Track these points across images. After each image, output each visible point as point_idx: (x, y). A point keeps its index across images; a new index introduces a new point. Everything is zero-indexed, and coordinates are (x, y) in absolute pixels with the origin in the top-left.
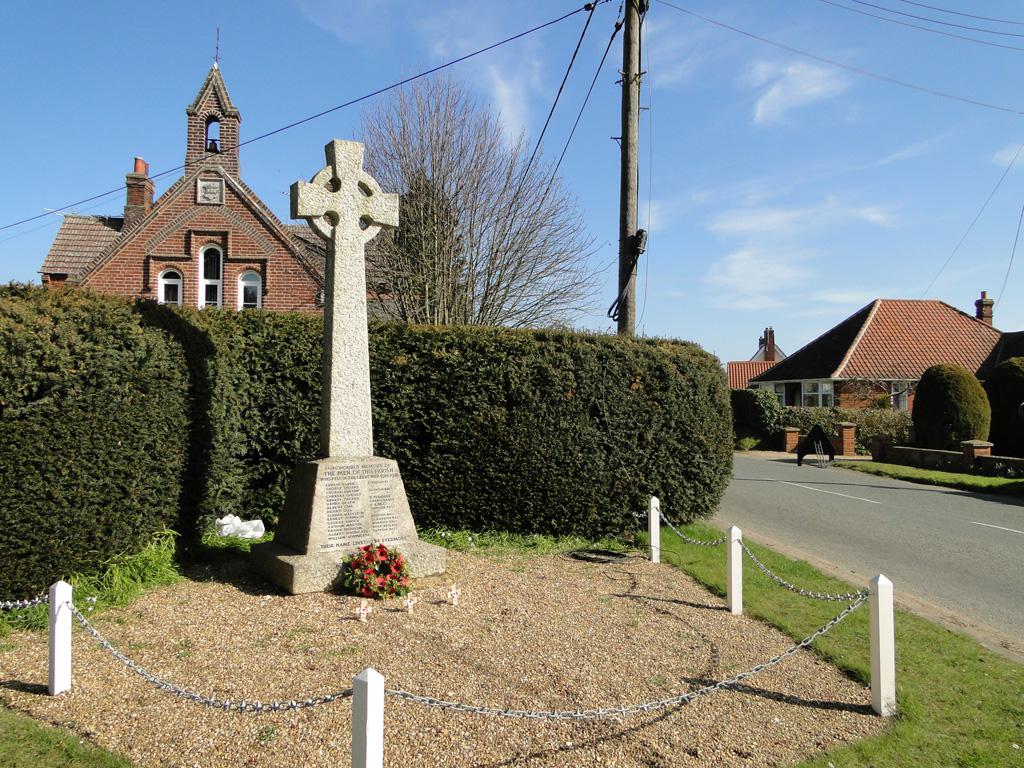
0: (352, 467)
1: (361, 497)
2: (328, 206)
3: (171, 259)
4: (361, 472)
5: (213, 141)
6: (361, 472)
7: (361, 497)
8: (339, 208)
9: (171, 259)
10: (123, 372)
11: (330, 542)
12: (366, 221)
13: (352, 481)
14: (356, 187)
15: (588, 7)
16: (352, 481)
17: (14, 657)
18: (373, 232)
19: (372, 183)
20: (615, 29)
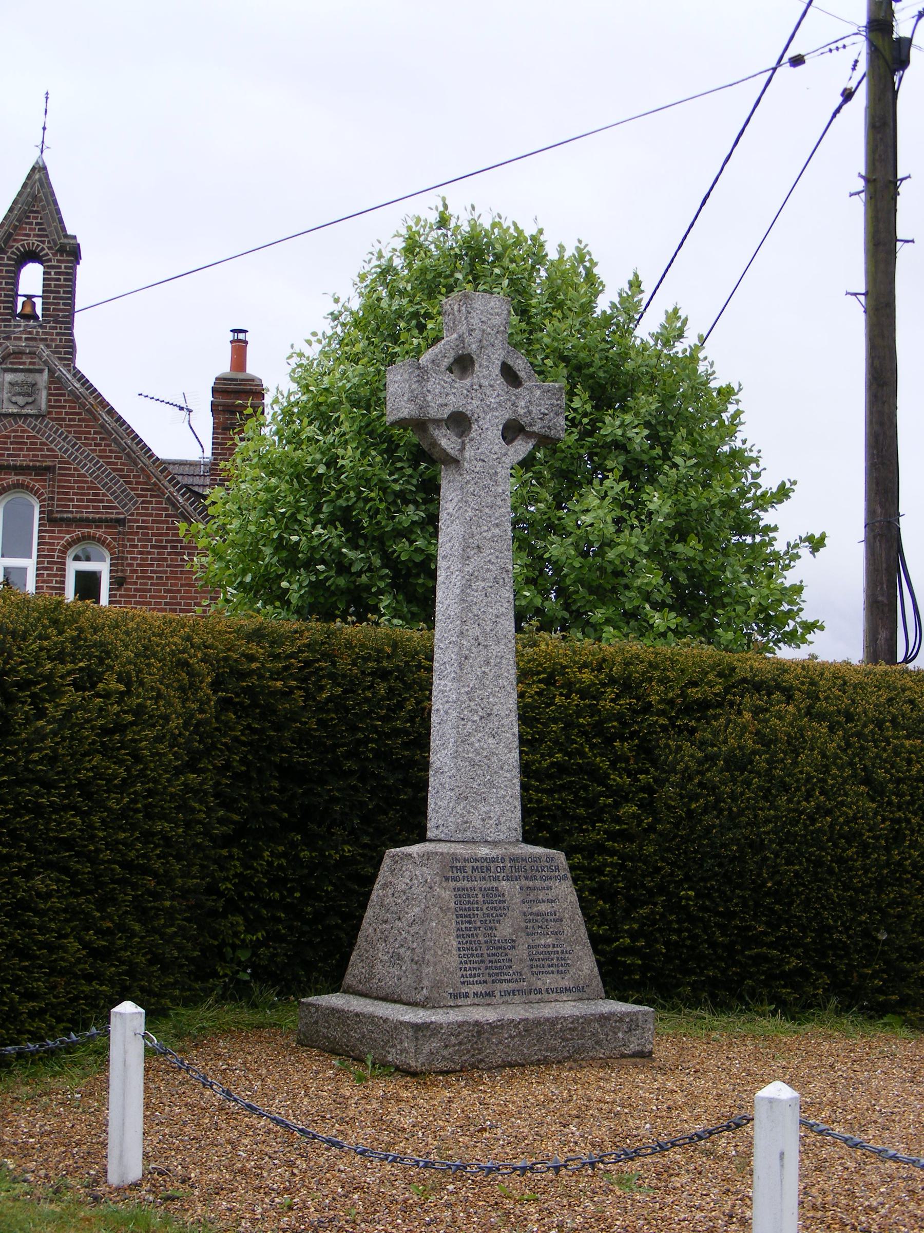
0: (493, 860)
1: (510, 913)
2: (455, 403)
3: (87, 522)
4: (508, 870)
5: (30, 297)
6: (508, 870)
7: (510, 913)
8: (471, 407)
9: (87, 522)
10: (251, 612)
11: (465, 989)
12: (512, 430)
13: (495, 884)
14: (497, 371)
15: (797, 61)
16: (495, 884)
17: (31, 1115)
18: (521, 448)
19: (520, 365)
20: (841, 99)
